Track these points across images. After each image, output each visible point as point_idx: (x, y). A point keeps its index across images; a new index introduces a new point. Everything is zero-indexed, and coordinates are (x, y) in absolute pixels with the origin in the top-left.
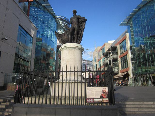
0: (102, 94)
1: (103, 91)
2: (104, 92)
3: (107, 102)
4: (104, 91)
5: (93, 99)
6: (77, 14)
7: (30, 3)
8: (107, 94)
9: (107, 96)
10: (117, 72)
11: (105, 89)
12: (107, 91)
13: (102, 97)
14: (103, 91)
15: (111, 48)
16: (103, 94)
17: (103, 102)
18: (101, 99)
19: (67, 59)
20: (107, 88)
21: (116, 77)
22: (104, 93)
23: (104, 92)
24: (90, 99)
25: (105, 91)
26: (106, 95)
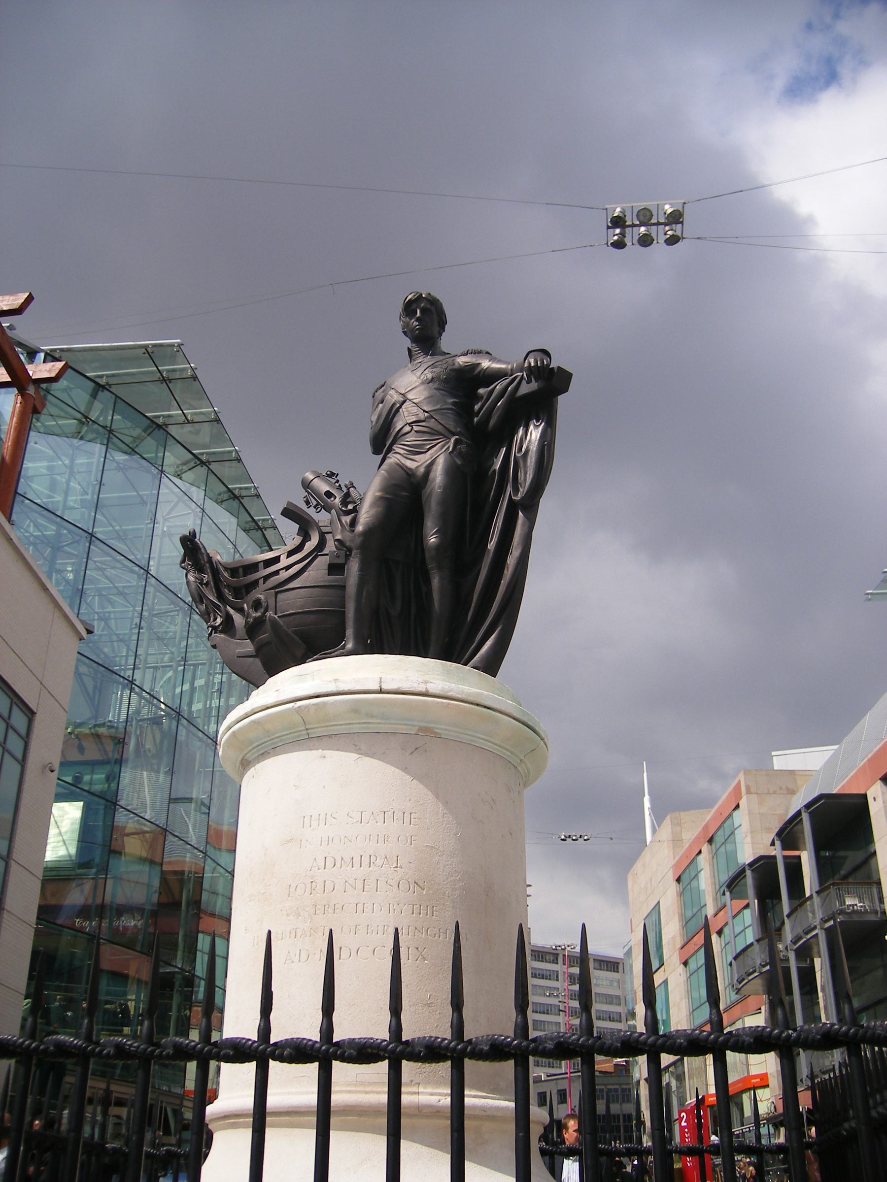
7: (31, 390)
15: (805, 817)
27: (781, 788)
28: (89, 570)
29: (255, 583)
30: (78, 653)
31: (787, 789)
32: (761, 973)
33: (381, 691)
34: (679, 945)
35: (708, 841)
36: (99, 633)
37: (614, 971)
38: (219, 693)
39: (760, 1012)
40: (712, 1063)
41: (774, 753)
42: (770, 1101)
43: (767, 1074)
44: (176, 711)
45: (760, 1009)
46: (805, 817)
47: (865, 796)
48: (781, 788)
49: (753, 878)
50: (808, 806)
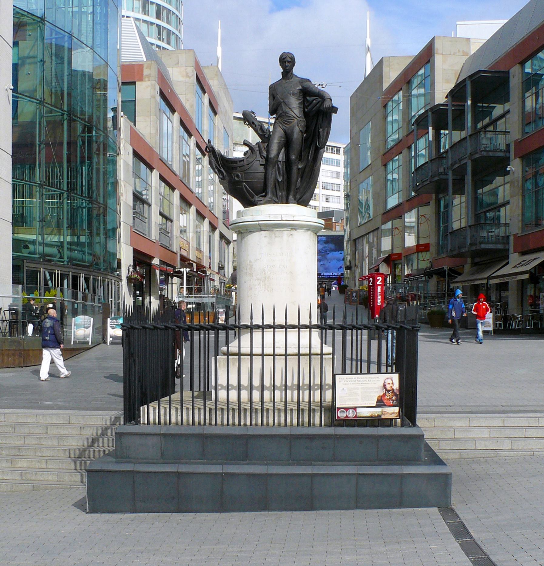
0: (382, 394)
1: (384, 386)
2: (386, 390)
3: (394, 416)
4: (388, 387)
5: (355, 408)
6: (296, 71)
8: (395, 394)
9: (396, 400)
10: (500, 247)
11: (389, 381)
12: (396, 386)
13: (380, 403)
14: (384, 386)
16: (384, 395)
17: (383, 417)
18: (377, 411)
19: (264, 270)
20: (396, 377)
21: (489, 278)
22: (389, 391)
23: (386, 390)
24: (347, 409)
25: (391, 385)
26: (394, 398)
27: (459, 51)
28: (74, 7)
29: (236, 168)
30: (14, 6)
31: (463, 51)
32: (431, 182)
33: (282, 220)
34: (382, 152)
35: (407, 83)
36: (357, 288)
37: (337, 166)
38: (92, 15)
39: (429, 205)
40: (411, 509)
41: (458, 23)
42: (429, 261)
43: (429, 244)
44: (69, 34)
45: (429, 202)
46: (469, 83)
47: (508, 72)
48: (459, 51)
49: (432, 117)
50: (470, 77)
